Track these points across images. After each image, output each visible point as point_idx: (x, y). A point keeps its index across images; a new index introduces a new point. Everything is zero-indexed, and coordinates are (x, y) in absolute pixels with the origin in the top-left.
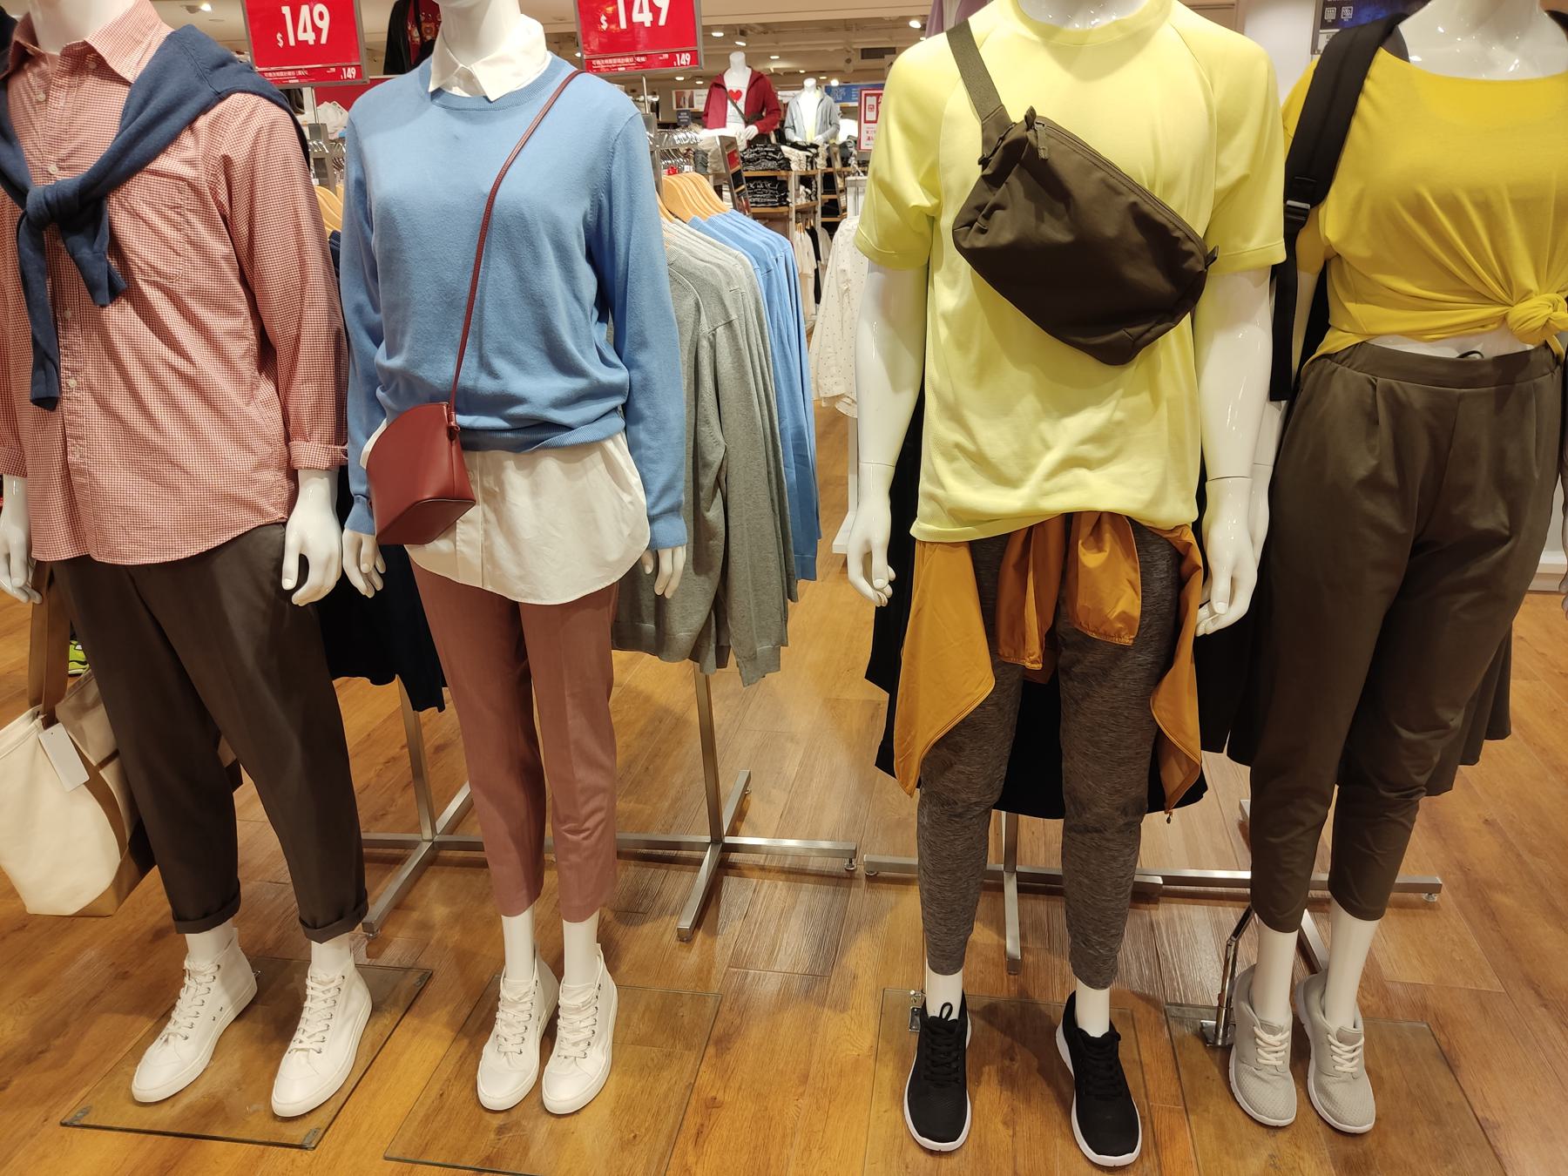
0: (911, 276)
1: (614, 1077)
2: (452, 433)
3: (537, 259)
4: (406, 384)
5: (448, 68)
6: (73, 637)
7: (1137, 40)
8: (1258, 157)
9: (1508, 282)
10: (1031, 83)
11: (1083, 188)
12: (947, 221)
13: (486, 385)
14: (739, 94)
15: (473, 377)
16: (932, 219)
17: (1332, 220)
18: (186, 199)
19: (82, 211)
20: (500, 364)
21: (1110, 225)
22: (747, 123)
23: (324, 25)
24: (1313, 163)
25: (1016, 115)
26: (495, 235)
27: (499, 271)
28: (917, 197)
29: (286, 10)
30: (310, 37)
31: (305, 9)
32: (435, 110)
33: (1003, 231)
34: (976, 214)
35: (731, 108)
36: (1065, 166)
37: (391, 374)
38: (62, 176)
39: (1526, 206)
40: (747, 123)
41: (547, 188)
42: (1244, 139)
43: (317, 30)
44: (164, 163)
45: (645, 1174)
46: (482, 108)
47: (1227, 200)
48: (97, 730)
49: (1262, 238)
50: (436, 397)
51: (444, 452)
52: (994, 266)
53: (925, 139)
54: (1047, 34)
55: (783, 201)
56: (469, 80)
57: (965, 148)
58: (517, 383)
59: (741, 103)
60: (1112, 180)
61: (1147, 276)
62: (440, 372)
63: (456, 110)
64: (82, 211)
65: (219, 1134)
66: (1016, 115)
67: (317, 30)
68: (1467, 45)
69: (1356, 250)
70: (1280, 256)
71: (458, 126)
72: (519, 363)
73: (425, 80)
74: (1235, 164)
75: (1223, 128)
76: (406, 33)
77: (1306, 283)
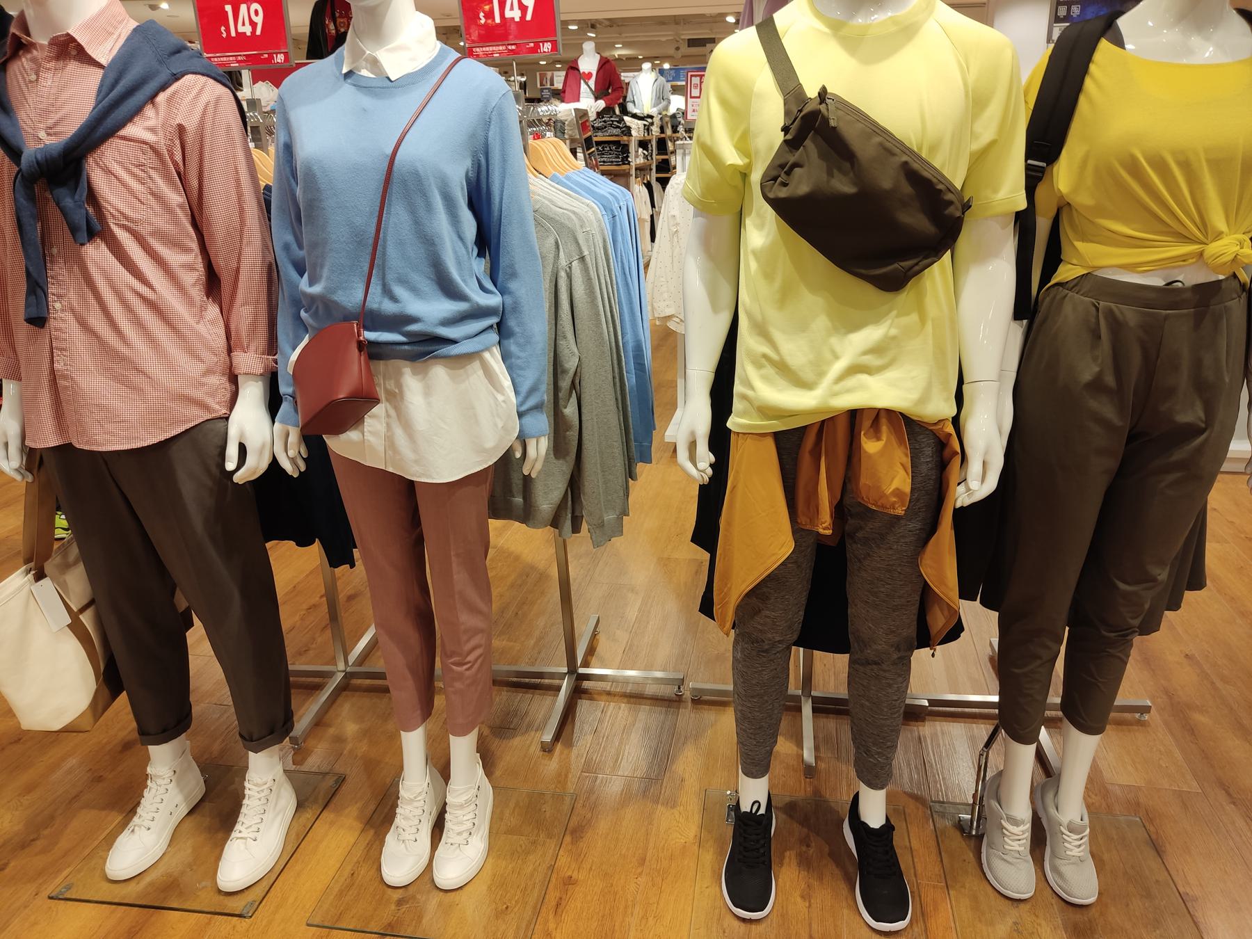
0: (727, 221)
1: (490, 860)
2: (361, 345)
3: (429, 207)
4: (324, 307)
5: (357, 54)
6: (58, 509)
7: (908, 32)
8: (1005, 126)
9: (1204, 225)
10: (823, 66)
11: (865, 150)
12: (756, 177)
13: (388, 307)
14: (590, 75)
15: (377, 301)
16: (744, 175)
17: (1064, 176)
18: (149, 159)
19: (66, 169)
20: (399, 291)
21: (886, 179)
22: (597, 98)
23: (259, 20)
24: (1048, 130)
25: (812, 92)
26: (395, 188)
27: (398, 217)
28: (732, 157)
29: (228, 8)
30: (247, 30)
31: (243, 7)
32: (347, 88)
33: (801, 185)
34: (780, 171)
35: (583, 86)
36: (851, 133)
37: (313, 299)
38: (49, 141)
39: (1218, 164)
40: (597, 98)
41: (437, 150)
42: (993, 111)
43: (253, 24)
44: (131, 130)
45: (515, 937)
46: (385, 87)
47: (980, 159)
48: (78, 583)
49: (1008, 190)
50: (348, 317)
51: (355, 361)
52: (794, 213)
53: (739, 111)
54: (836, 27)
56: (375, 64)
57: (771, 118)
58: (413, 306)
59: (592, 83)
60: (888, 144)
61: (916, 220)
62: (351, 297)
63: (364, 87)
64: (66, 169)
65: (175, 905)
66: (812, 92)
67: (253, 24)
68: (1171, 36)
69: (1083, 200)
70: (1022, 205)
71: (366, 101)
72: (414, 290)
73: (339, 64)
74: (986, 131)
75: (976, 102)
76: (324, 26)
77: (1043, 226)
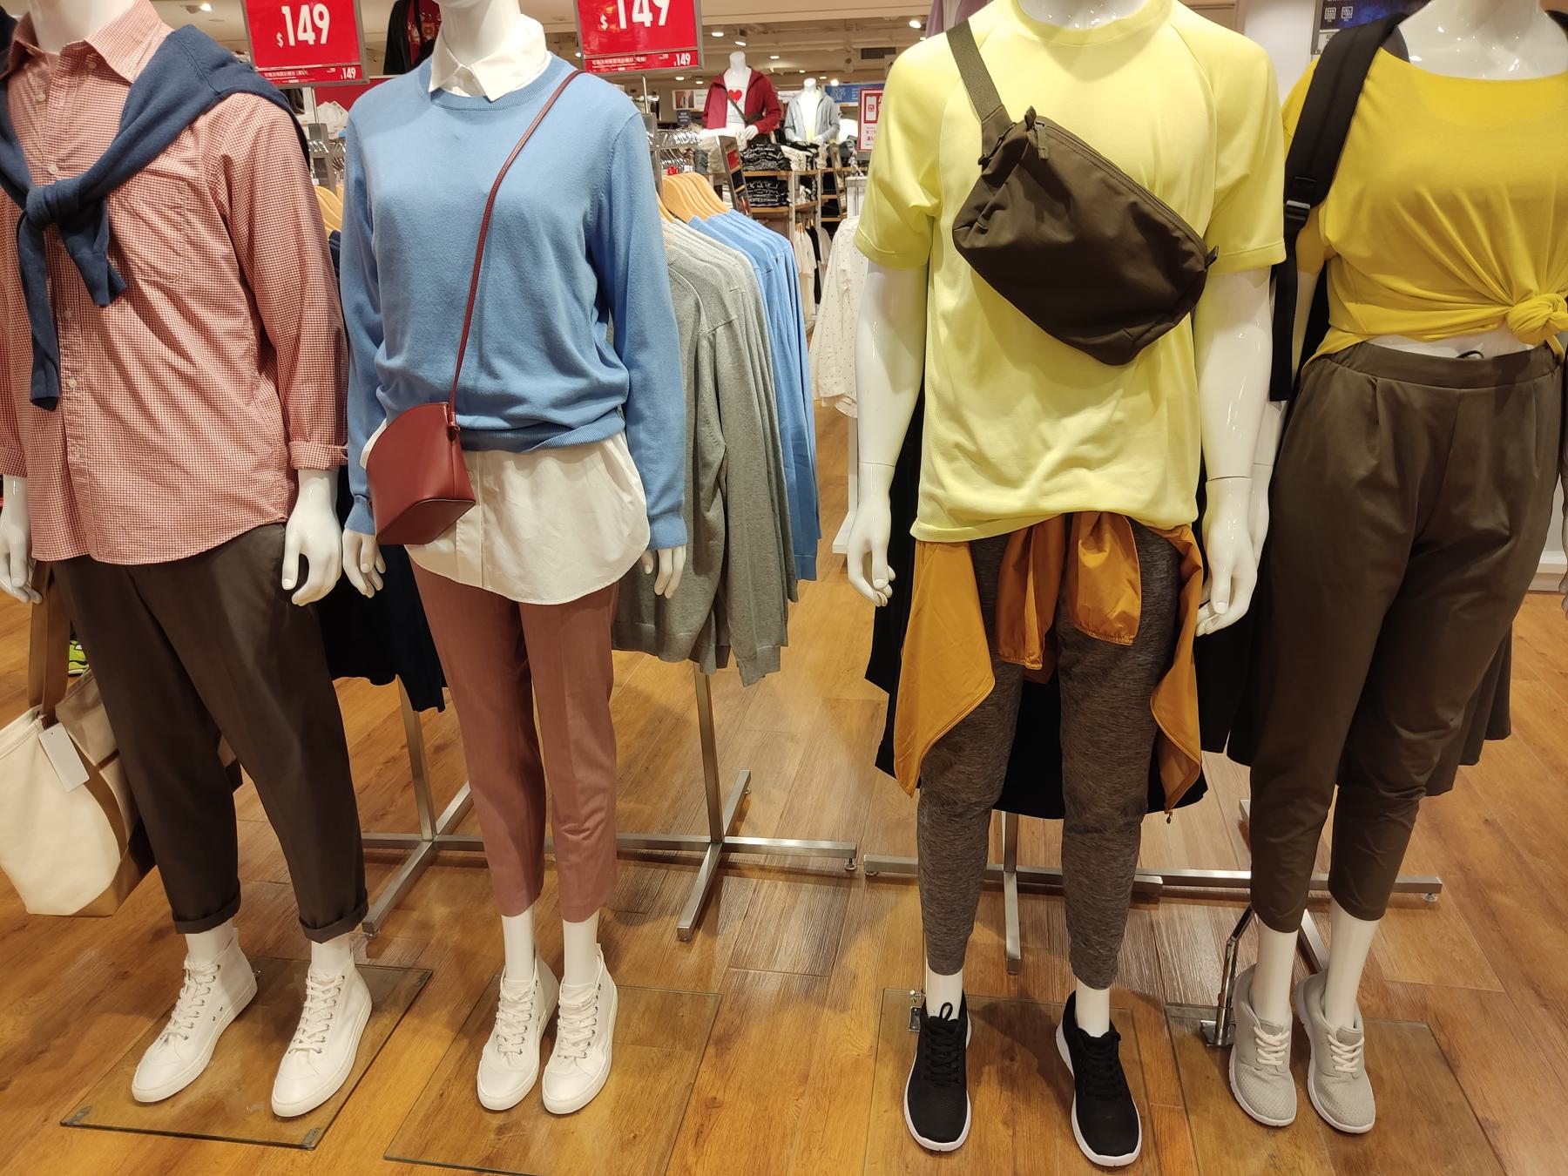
0: (911, 276)
1: (614, 1077)
2: (452, 433)
3: (537, 259)
4: (406, 384)
5: (448, 68)
7: (1137, 40)
8: (1258, 157)
9: (1508, 282)
10: (1031, 83)
11: (1083, 188)
12: (947, 221)
13: (486, 385)
14: (739, 94)
15: (473, 377)
16: (932, 219)
17: (1332, 220)
18: (186, 199)
19: (82, 211)
20: (500, 364)
21: (1110, 225)
22: (747, 123)
23: (324, 25)
24: (1313, 163)
25: (1016, 115)
26: (495, 235)
27: (499, 271)
28: (917, 197)
29: (286, 10)
30: (310, 37)
31: (305, 9)
32: (435, 110)
33: (1003, 231)
34: (976, 214)
35: (731, 108)
36: (1065, 166)
37: (391, 374)
38: (62, 176)
39: (1526, 206)
40: (747, 123)
41: (547, 188)
42: (1244, 139)
43: (317, 30)
44: (164, 163)
45: (645, 1174)
46: (482, 108)
47: (1227, 200)
49: (1262, 238)
50: (436, 397)
51: (444, 452)
52: (994, 266)
53: (925, 139)
54: (1047, 34)
55: (783, 201)
56: (469, 80)
57: (965, 148)
58: (517, 383)
59: (741, 103)
60: (1112, 180)
61: (1147, 276)
62: (440, 372)
63: (456, 110)
64: (82, 211)
65: (219, 1134)
66: (1016, 115)
67: (317, 30)
68: (1467, 45)
69: (1356, 250)
70: (1280, 256)
71: (458, 126)
72: (519, 363)
73: (425, 80)
74: (1235, 164)
75: (1223, 128)
76: (406, 33)
77: (1306, 283)
